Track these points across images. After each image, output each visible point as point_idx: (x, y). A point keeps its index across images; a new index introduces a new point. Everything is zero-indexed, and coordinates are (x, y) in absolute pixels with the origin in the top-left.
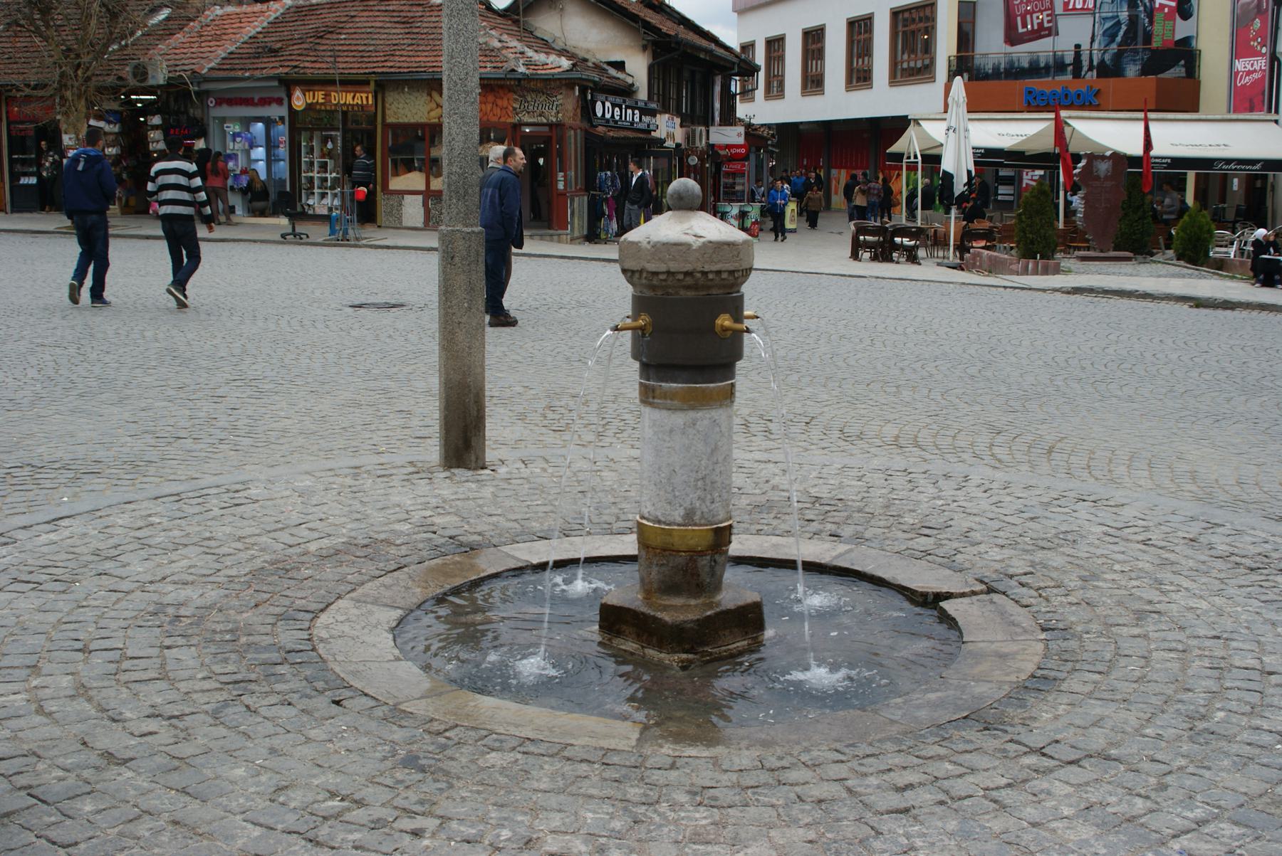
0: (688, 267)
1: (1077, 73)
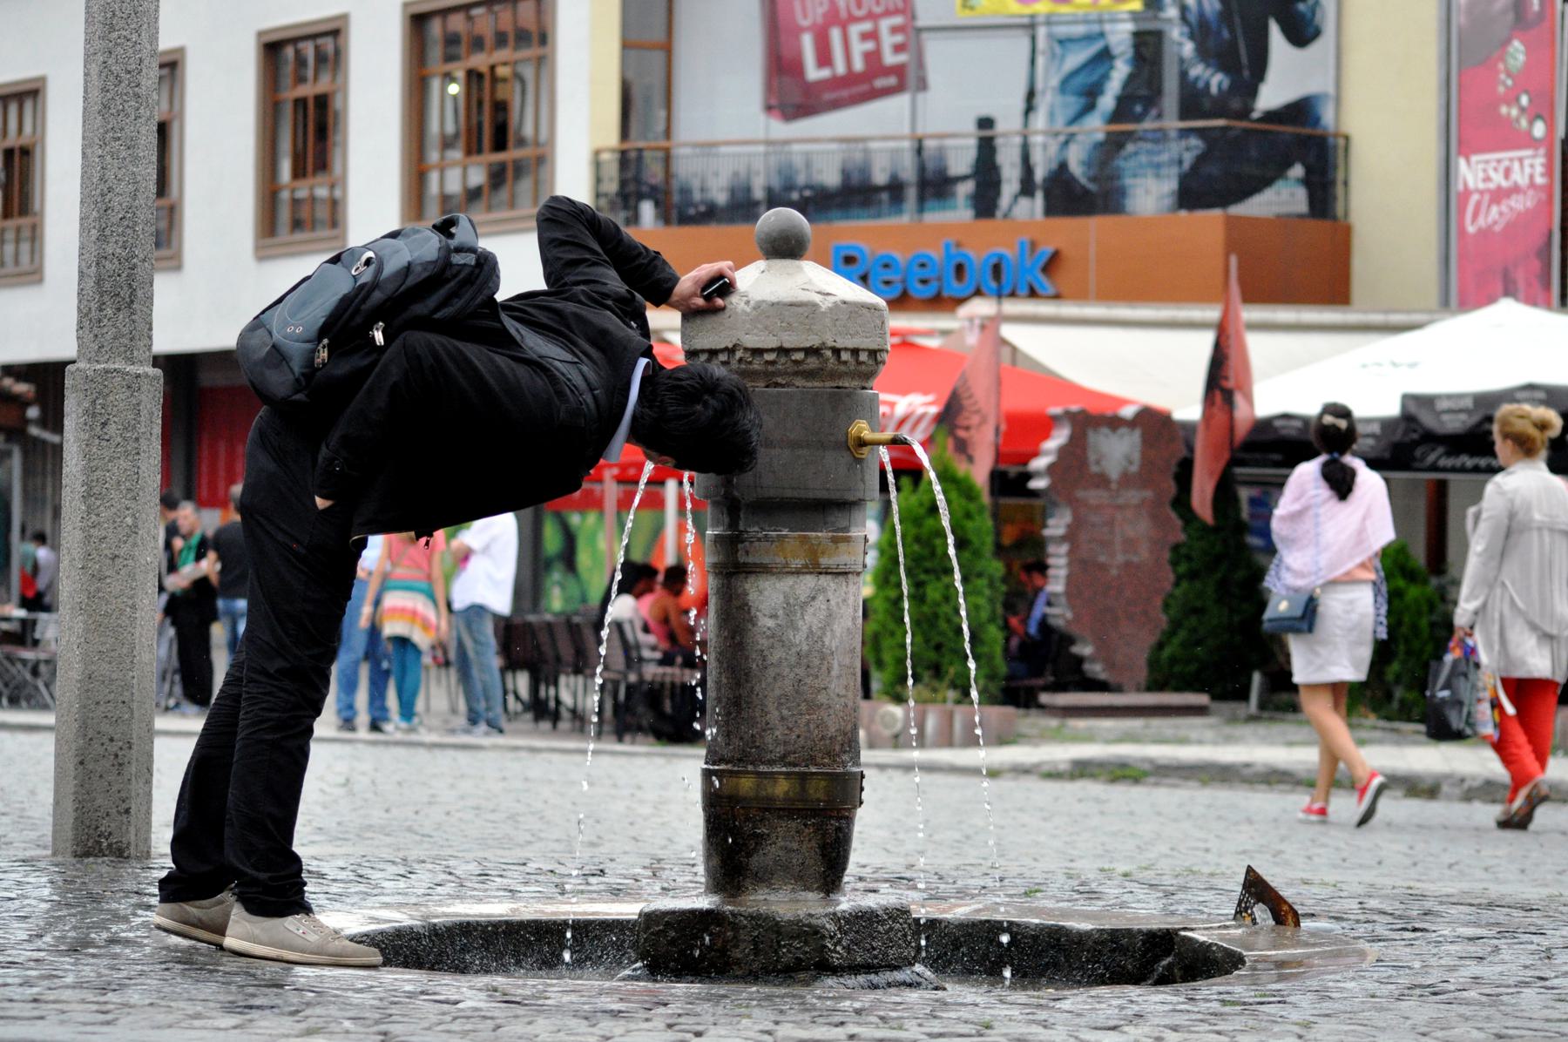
0: (812, 341)
1: (985, 202)
